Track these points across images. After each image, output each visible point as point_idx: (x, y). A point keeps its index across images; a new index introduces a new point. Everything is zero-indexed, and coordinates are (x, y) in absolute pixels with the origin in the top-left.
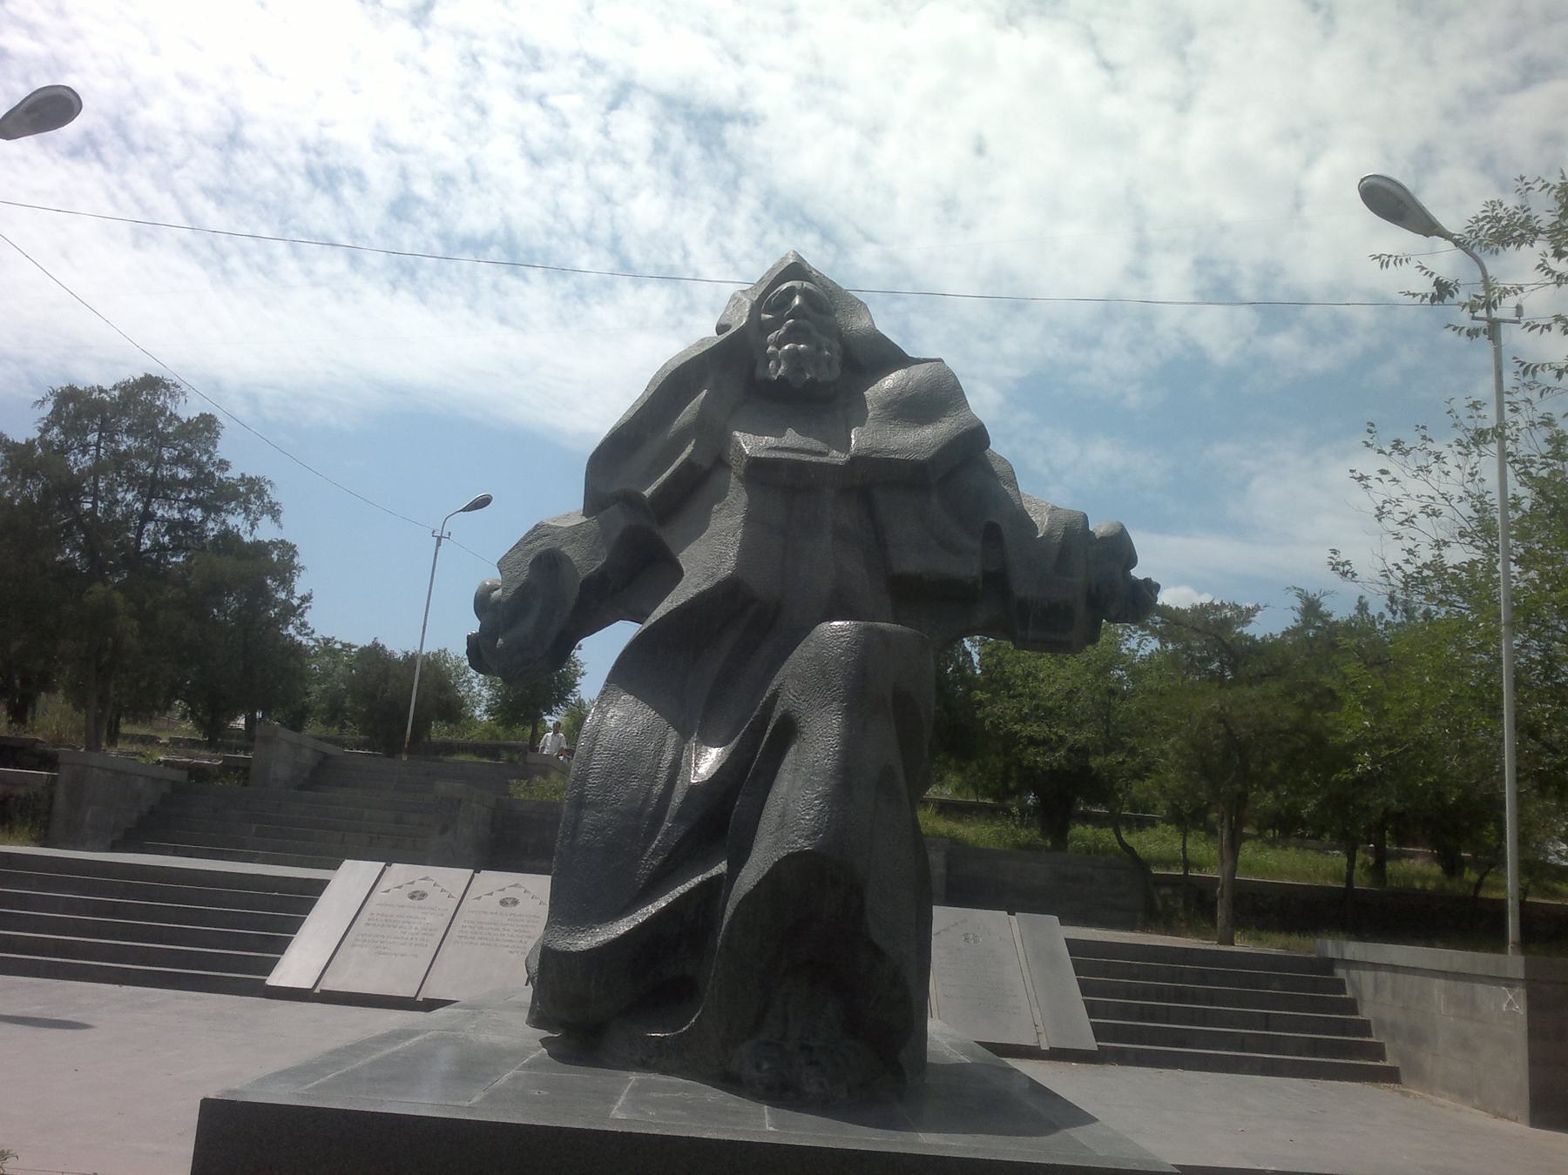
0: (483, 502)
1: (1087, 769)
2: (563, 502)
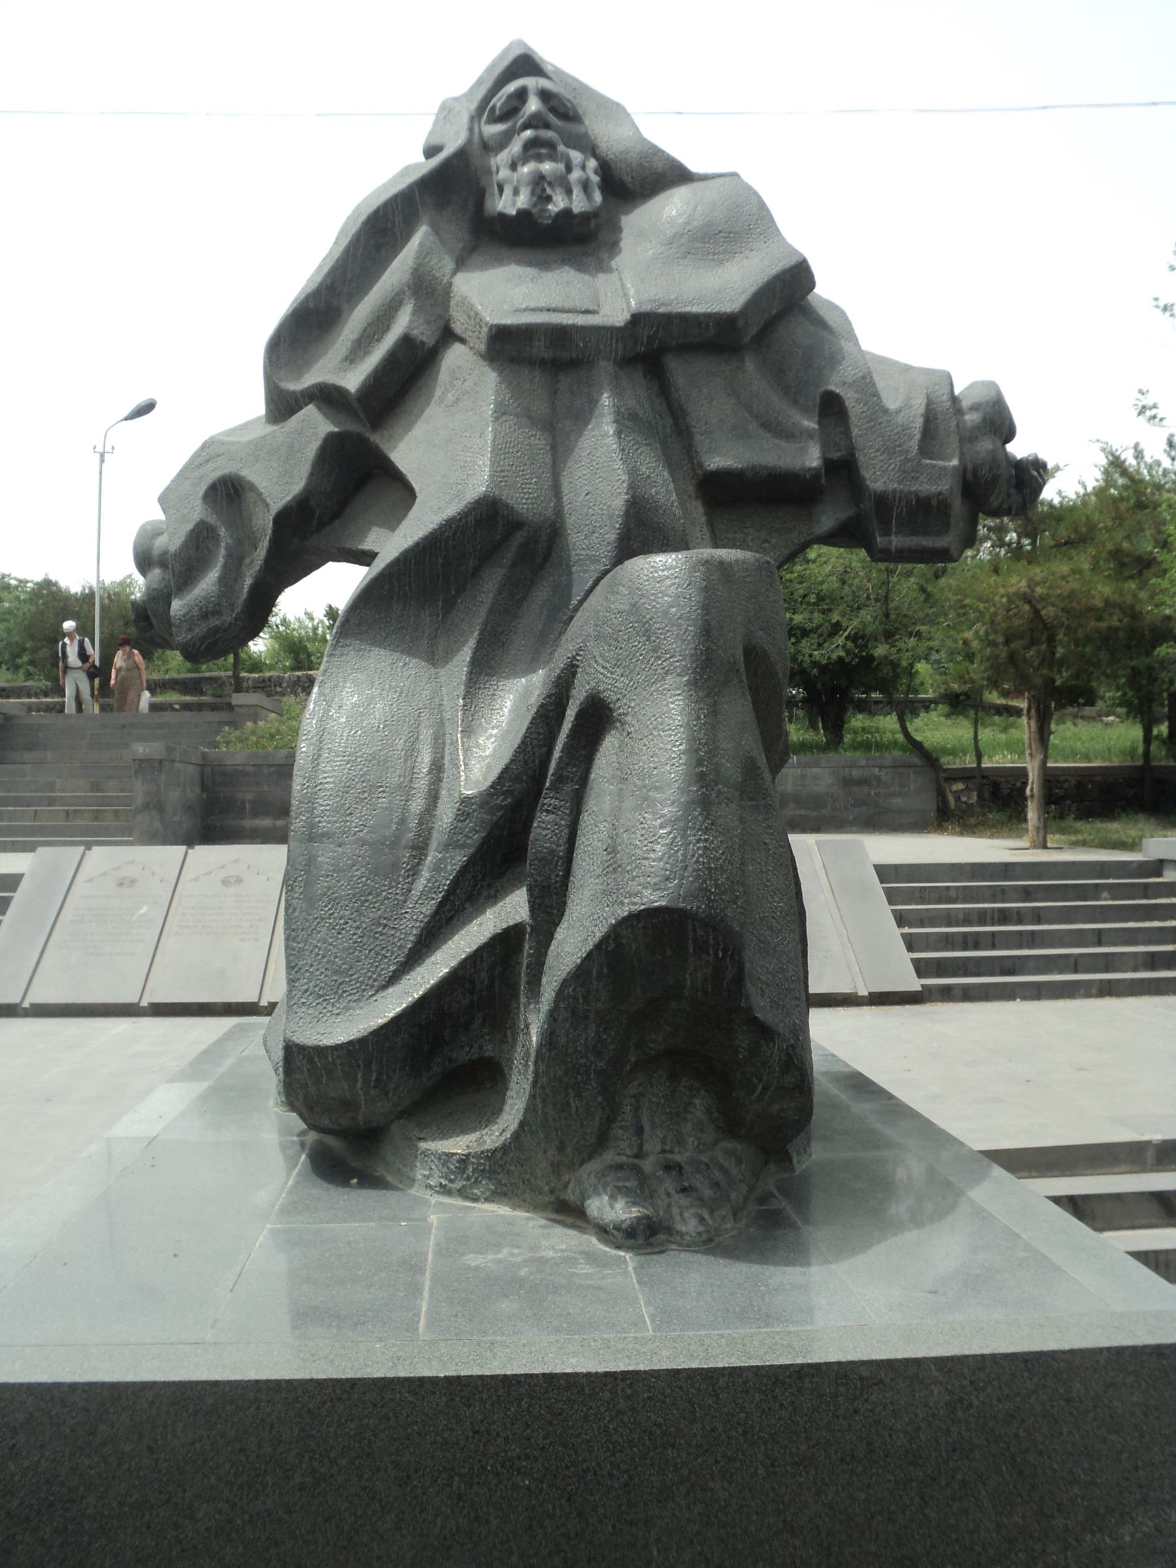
0: (147, 408)
1: (871, 658)
2: (220, 396)
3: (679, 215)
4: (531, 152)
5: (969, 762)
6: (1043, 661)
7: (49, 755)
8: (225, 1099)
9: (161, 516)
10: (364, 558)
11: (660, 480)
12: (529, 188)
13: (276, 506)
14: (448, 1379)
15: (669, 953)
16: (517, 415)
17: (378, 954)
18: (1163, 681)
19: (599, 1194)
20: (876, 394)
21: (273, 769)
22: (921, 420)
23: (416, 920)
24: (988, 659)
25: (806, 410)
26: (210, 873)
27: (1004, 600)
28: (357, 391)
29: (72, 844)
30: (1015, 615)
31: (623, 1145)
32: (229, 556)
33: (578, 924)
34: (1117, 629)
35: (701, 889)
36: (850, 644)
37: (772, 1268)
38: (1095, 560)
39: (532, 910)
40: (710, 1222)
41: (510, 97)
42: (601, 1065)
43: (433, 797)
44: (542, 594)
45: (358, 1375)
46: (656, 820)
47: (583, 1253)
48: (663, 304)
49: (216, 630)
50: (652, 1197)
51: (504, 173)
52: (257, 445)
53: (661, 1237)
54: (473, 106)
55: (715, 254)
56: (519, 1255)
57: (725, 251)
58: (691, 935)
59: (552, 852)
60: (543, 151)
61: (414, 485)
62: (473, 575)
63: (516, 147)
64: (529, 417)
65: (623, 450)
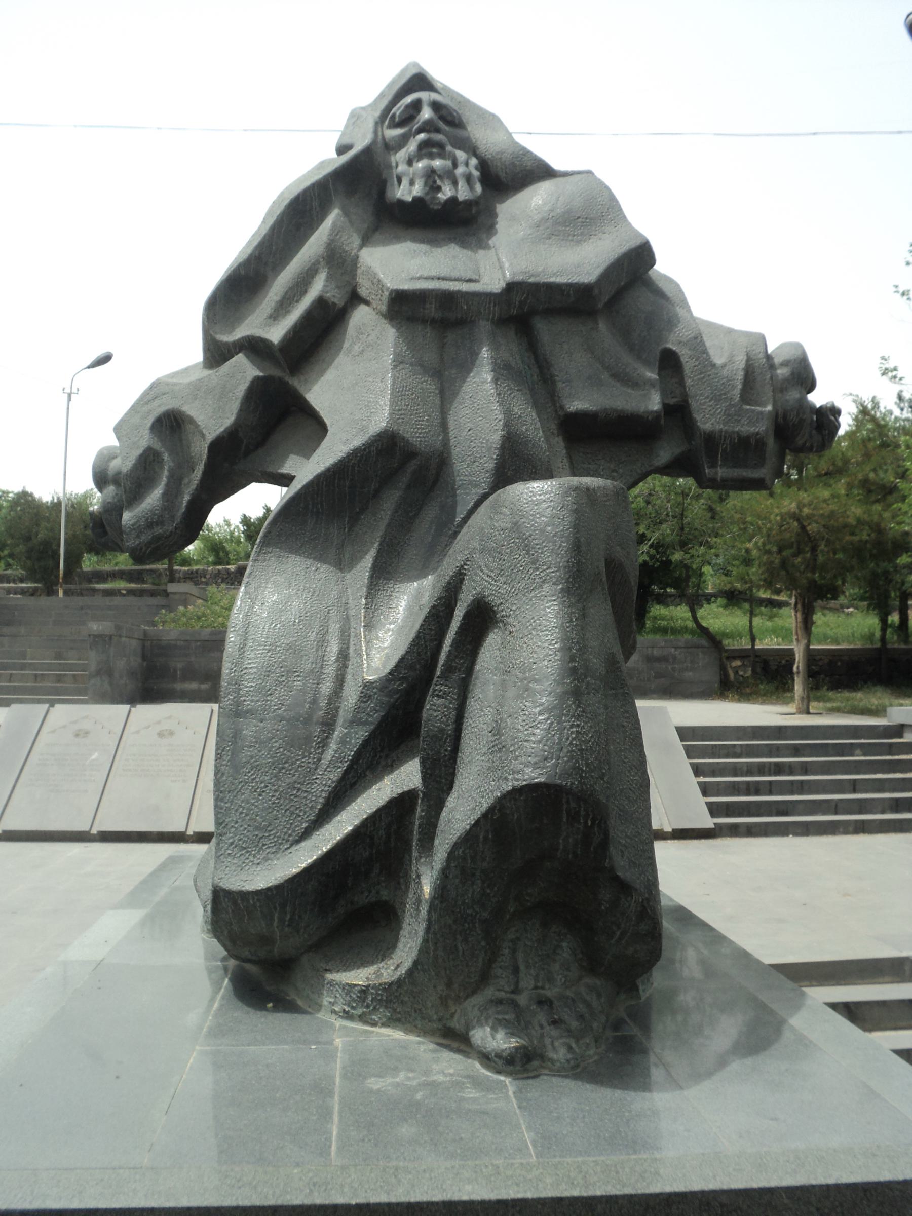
0: (105, 359)
1: (670, 562)
2: (166, 346)
3: (545, 204)
4: (424, 151)
5: (745, 644)
6: (807, 566)
7: (23, 630)
8: (161, 919)
9: (116, 443)
10: (284, 480)
11: (529, 419)
12: (423, 180)
13: (211, 436)
14: (359, 1207)
15: (545, 821)
16: (411, 365)
17: (292, 813)
18: (897, 582)
19: (482, 1026)
20: (705, 351)
21: (199, 644)
22: (742, 373)
23: (325, 785)
24: (765, 564)
25: (647, 363)
26: (149, 727)
27: (778, 518)
28: (280, 342)
29: (39, 701)
30: (786, 530)
31: (502, 982)
32: (171, 476)
33: (467, 795)
34: (866, 541)
35: (574, 768)
36: (653, 551)
37: (633, 1094)
38: (850, 486)
39: (424, 779)
40: (577, 1050)
41: (407, 107)
42: (485, 915)
43: (340, 681)
44: (430, 513)
45: (280, 1202)
46: (535, 707)
47: (468, 1077)
48: (532, 275)
49: (157, 538)
50: (527, 1027)
51: (402, 168)
52: (196, 390)
53: (535, 1063)
54: (378, 113)
55: (574, 236)
56: (414, 1078)
57: (582, 234)
58: (565, 806)
59: (442, 730)
60: (434, 150)
61: (326, 420)
62: (374, 496)
63: (412, 147)
64: (422, 366)
65: (499, 394)
